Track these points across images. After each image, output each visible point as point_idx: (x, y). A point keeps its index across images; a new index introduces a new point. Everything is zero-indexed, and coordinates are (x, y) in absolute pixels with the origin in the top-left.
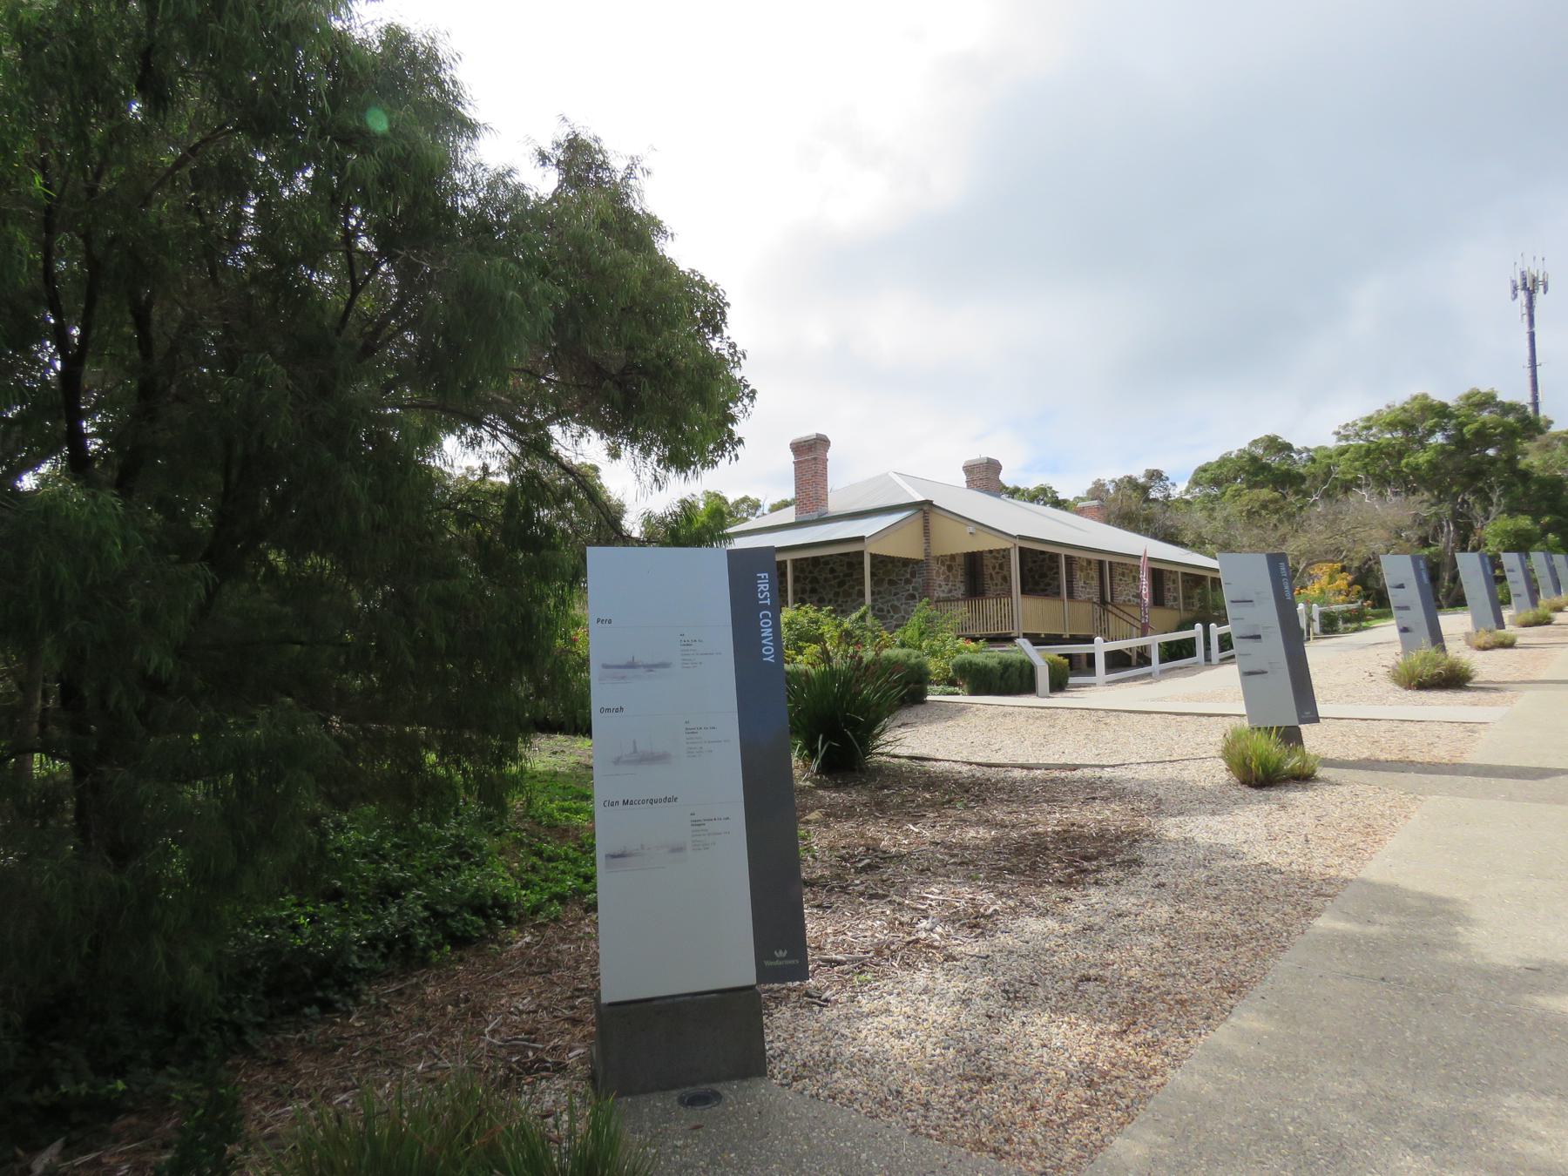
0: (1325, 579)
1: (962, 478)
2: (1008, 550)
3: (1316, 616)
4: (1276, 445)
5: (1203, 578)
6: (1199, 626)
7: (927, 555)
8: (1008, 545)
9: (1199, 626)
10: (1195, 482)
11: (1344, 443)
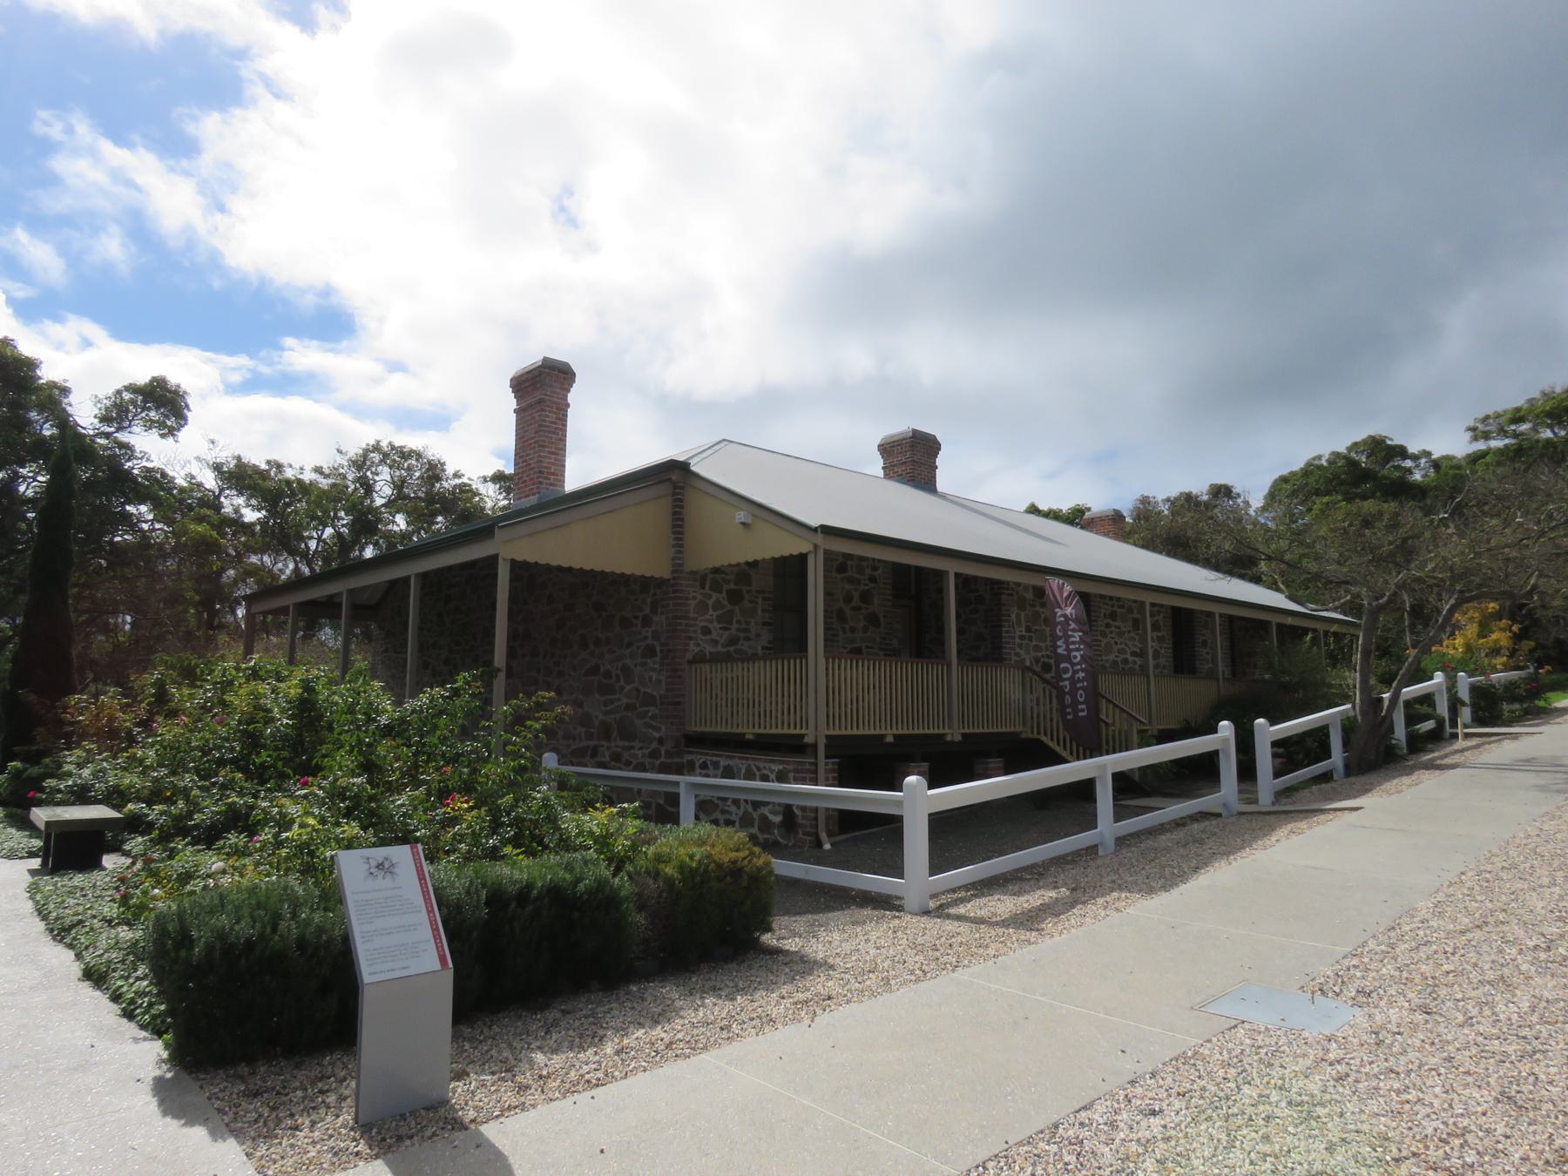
0: (1472, 630)
1: (876, 466)
2: (802, 558)
3: (1464, 694)
4: (1382, 450)
5: (1264, 625)
6: (1226, 727)
7: (677, 567)
8: (804, 547)
9: (1226, 727)
10: (1272, 496)
11: (1481, 446)
